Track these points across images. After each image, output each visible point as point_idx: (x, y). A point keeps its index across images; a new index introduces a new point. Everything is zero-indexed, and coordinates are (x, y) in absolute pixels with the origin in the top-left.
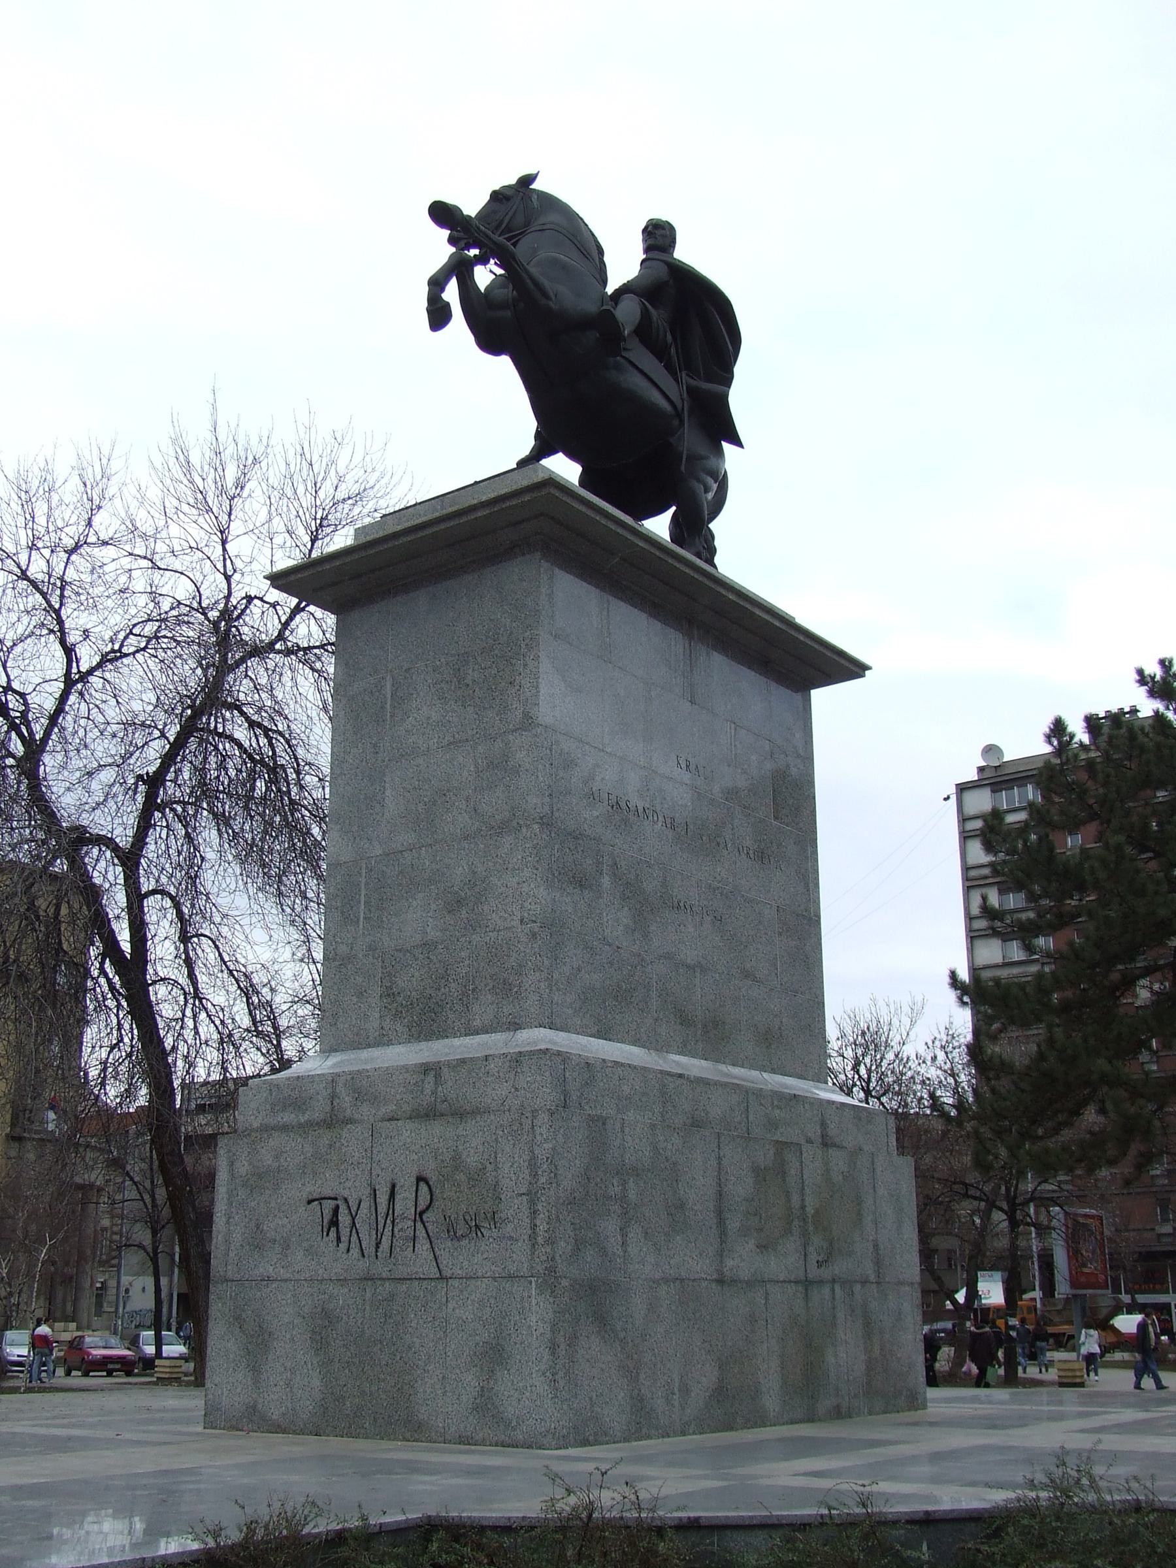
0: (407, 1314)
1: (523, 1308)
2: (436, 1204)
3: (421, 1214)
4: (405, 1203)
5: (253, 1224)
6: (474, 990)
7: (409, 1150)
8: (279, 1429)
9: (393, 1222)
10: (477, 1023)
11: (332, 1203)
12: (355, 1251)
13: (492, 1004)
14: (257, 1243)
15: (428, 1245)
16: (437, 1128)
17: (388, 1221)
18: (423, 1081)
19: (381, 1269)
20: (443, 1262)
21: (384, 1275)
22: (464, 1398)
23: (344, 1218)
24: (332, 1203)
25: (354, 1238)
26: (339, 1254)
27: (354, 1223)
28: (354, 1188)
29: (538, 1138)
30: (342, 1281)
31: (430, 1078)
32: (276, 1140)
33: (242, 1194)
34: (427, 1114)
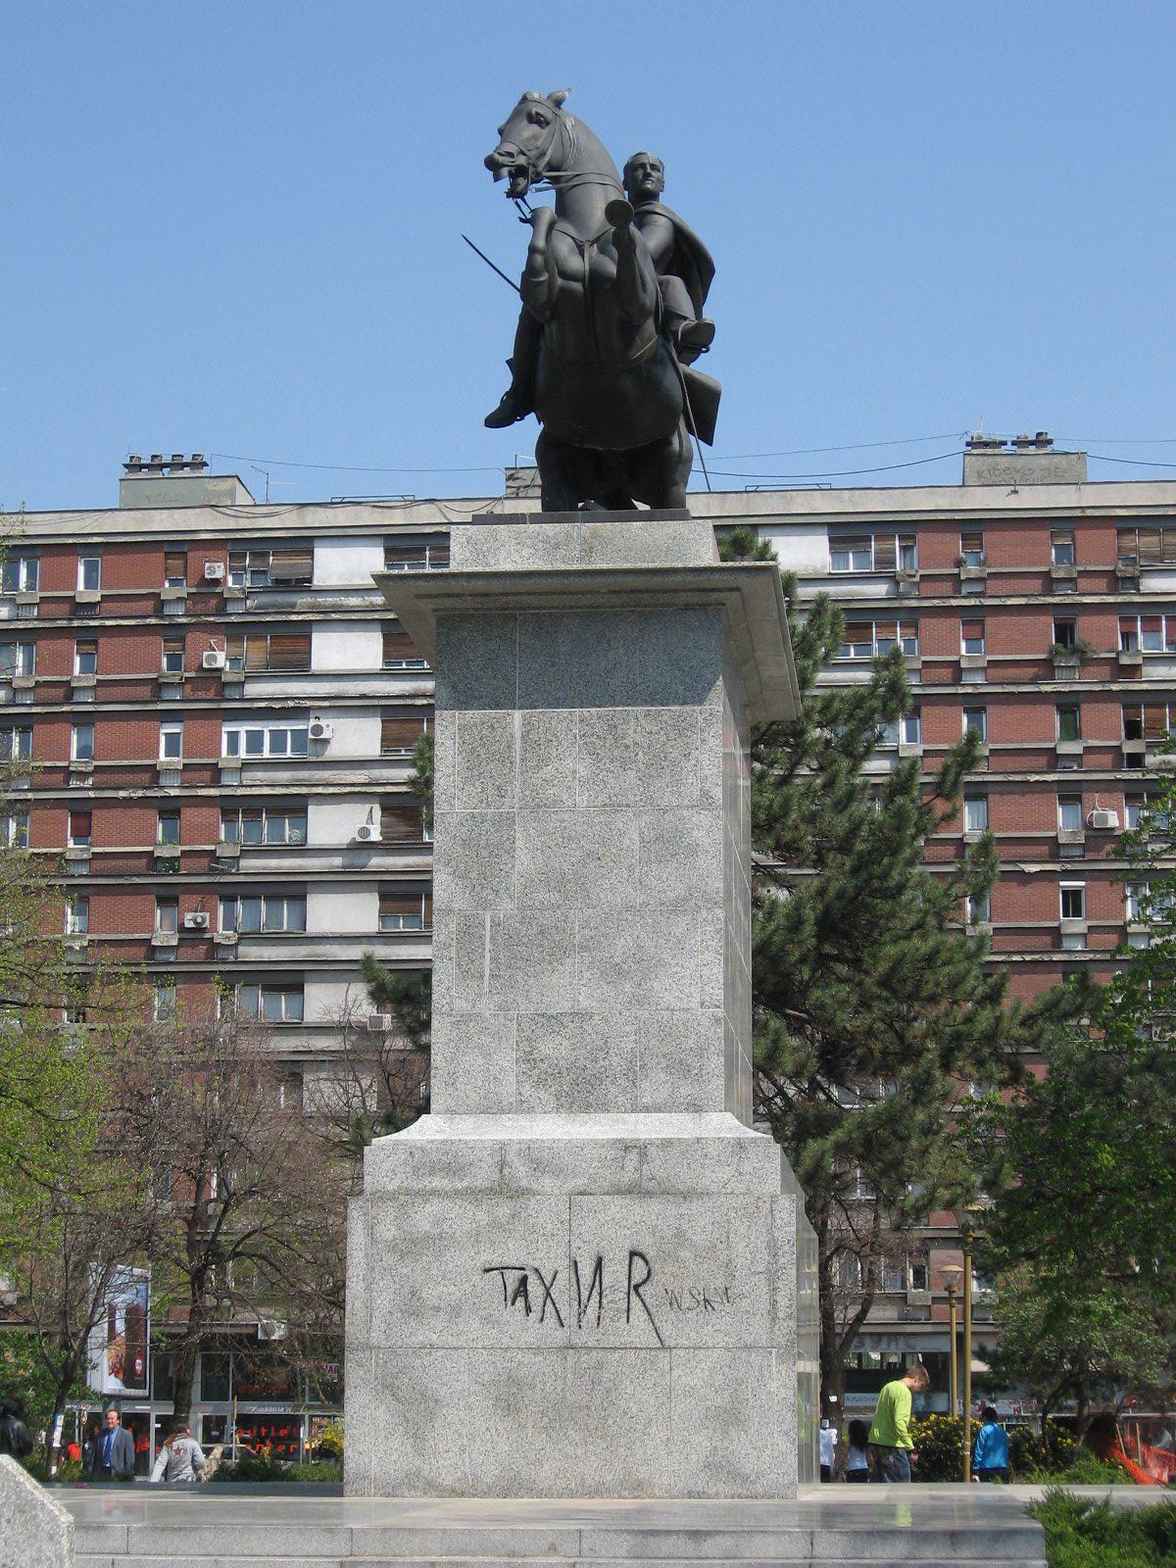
0: (621, 1382)
1: (762, 1376)
2: (655, 1278)
3: (636, 1287)
4: (615, 1275)
5: (406, 1291)
6: (642, 1067)
7: (615, 1227)
8: (455, 1493)
9: (601, 1294)
10: (647, 1100)
11: (519, 1274)
12: (551, 1321)
13: (666, 1082)
14: (413, 1307)
15: (646, 1316)
16: (655, 1206)
17: (594, 1293)
18: (624, 1158)
19: (586, 1337)
20: (665, 1333)
21: (590, 1344)
22: (694, 1458)
23: (534, 1288)
24: (519, 1274)
25: (549, 1307)
26: (530, 1324)
27: (548, 1294)
28: (549, 1259)
29: (779, 1221)
30: (537, 1350)
31: (633, 1155)
32: (434, 1207)
33: (389, 1259)
34: (634, 1190)
